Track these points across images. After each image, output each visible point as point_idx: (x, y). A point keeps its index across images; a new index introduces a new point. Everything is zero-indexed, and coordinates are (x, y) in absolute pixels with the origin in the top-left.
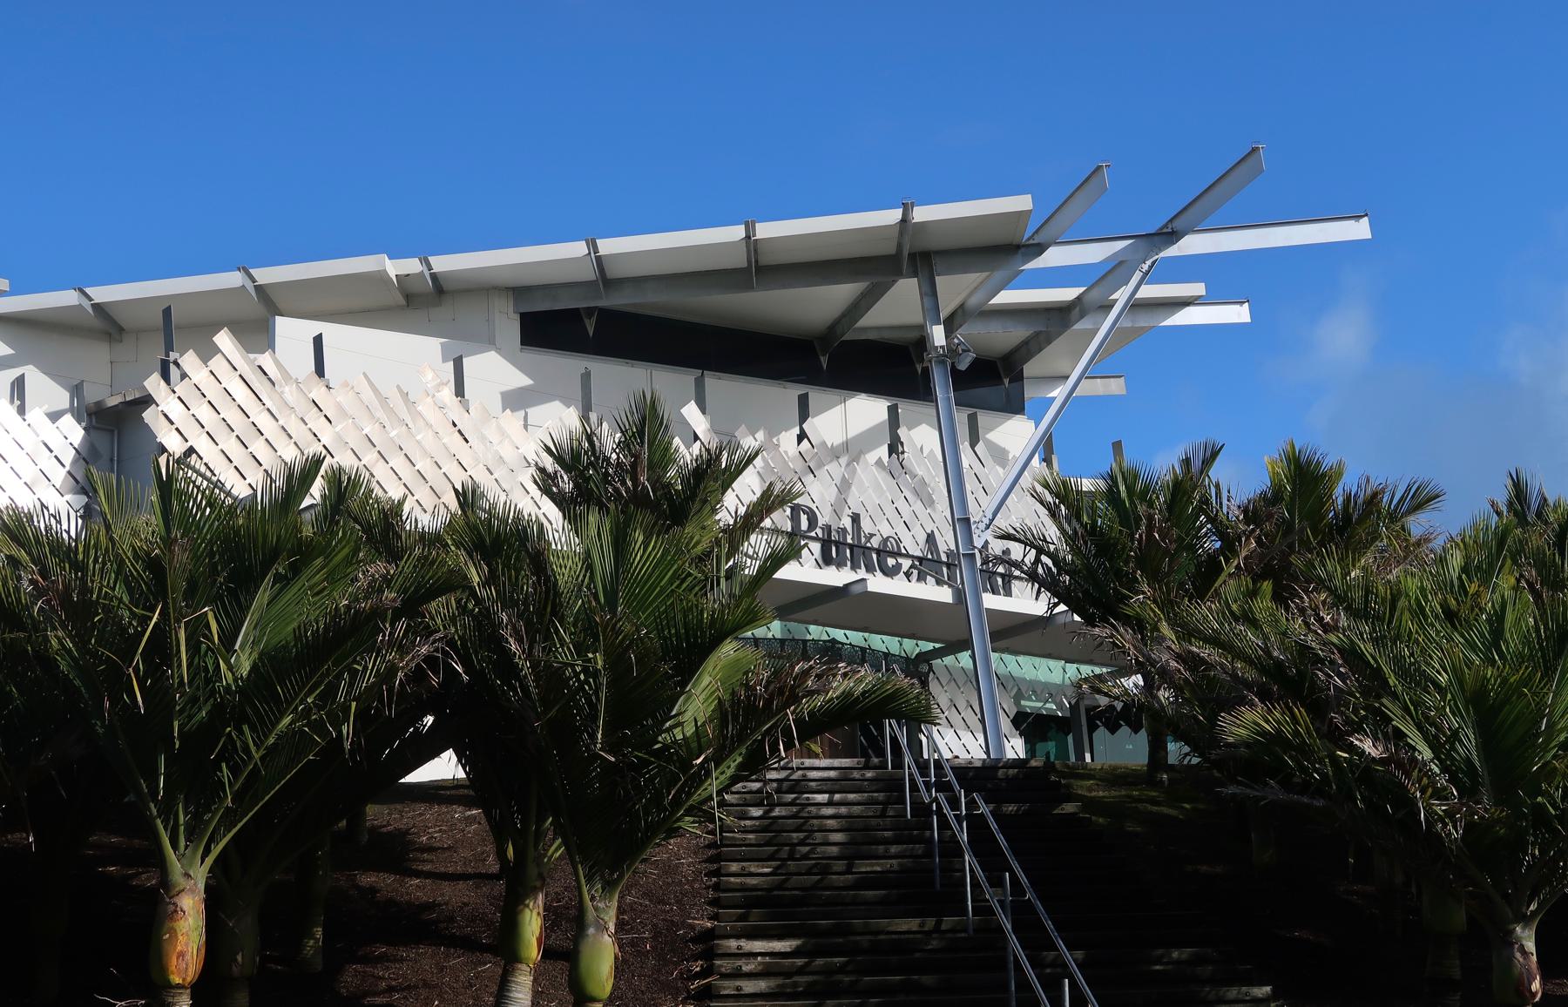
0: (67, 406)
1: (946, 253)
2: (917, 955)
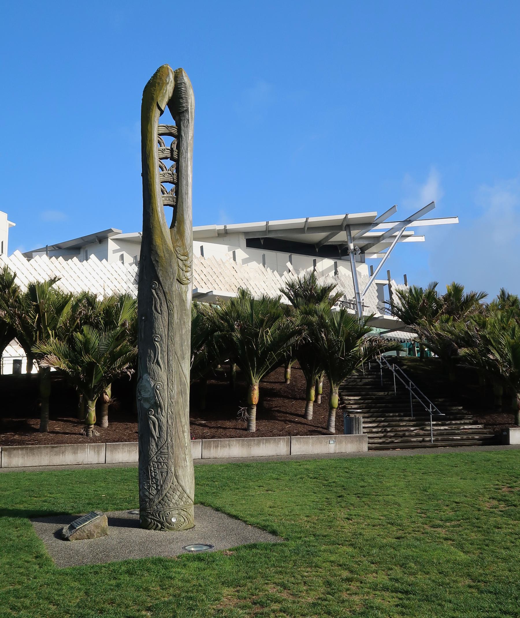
1: (351, 225)
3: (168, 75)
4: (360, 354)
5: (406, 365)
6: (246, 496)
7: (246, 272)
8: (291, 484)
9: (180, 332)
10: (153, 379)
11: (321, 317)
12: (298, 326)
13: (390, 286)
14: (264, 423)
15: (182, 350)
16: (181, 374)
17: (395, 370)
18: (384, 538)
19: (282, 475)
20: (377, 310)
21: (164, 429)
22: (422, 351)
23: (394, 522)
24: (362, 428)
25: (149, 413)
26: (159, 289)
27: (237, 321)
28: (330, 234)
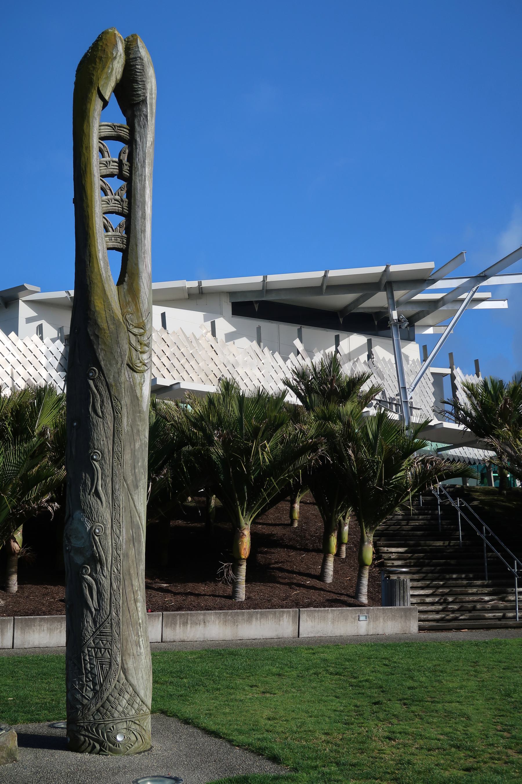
0: (56, 336)
2: (445, 553)
3: (115, 45)
4: (406, 483)
5: (477, 500)
6: (232, 700)
7: (232, 355)
8: (300, 683)
9: (132, 447)
10: (89, 518)
11: (347, 425)
12: (311, 438)
13: (453, 377)
14: (258, 587)
15: (135, 475)
16: (132, 512)
17: (460, 507)
18: (446, 769)
19: (287, 669)
20: (432, 414)
21: (107, 596)
22: (502, 478)
23: (460, 744)
24: (409, 596)
25: (82, 571)
26: (100, 379)
27: (218, 430)
28: (361, 296)
